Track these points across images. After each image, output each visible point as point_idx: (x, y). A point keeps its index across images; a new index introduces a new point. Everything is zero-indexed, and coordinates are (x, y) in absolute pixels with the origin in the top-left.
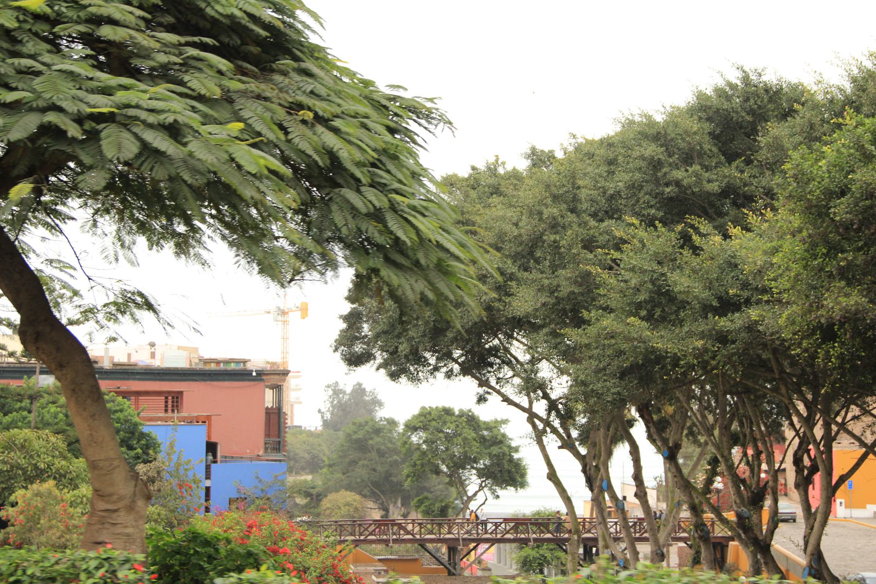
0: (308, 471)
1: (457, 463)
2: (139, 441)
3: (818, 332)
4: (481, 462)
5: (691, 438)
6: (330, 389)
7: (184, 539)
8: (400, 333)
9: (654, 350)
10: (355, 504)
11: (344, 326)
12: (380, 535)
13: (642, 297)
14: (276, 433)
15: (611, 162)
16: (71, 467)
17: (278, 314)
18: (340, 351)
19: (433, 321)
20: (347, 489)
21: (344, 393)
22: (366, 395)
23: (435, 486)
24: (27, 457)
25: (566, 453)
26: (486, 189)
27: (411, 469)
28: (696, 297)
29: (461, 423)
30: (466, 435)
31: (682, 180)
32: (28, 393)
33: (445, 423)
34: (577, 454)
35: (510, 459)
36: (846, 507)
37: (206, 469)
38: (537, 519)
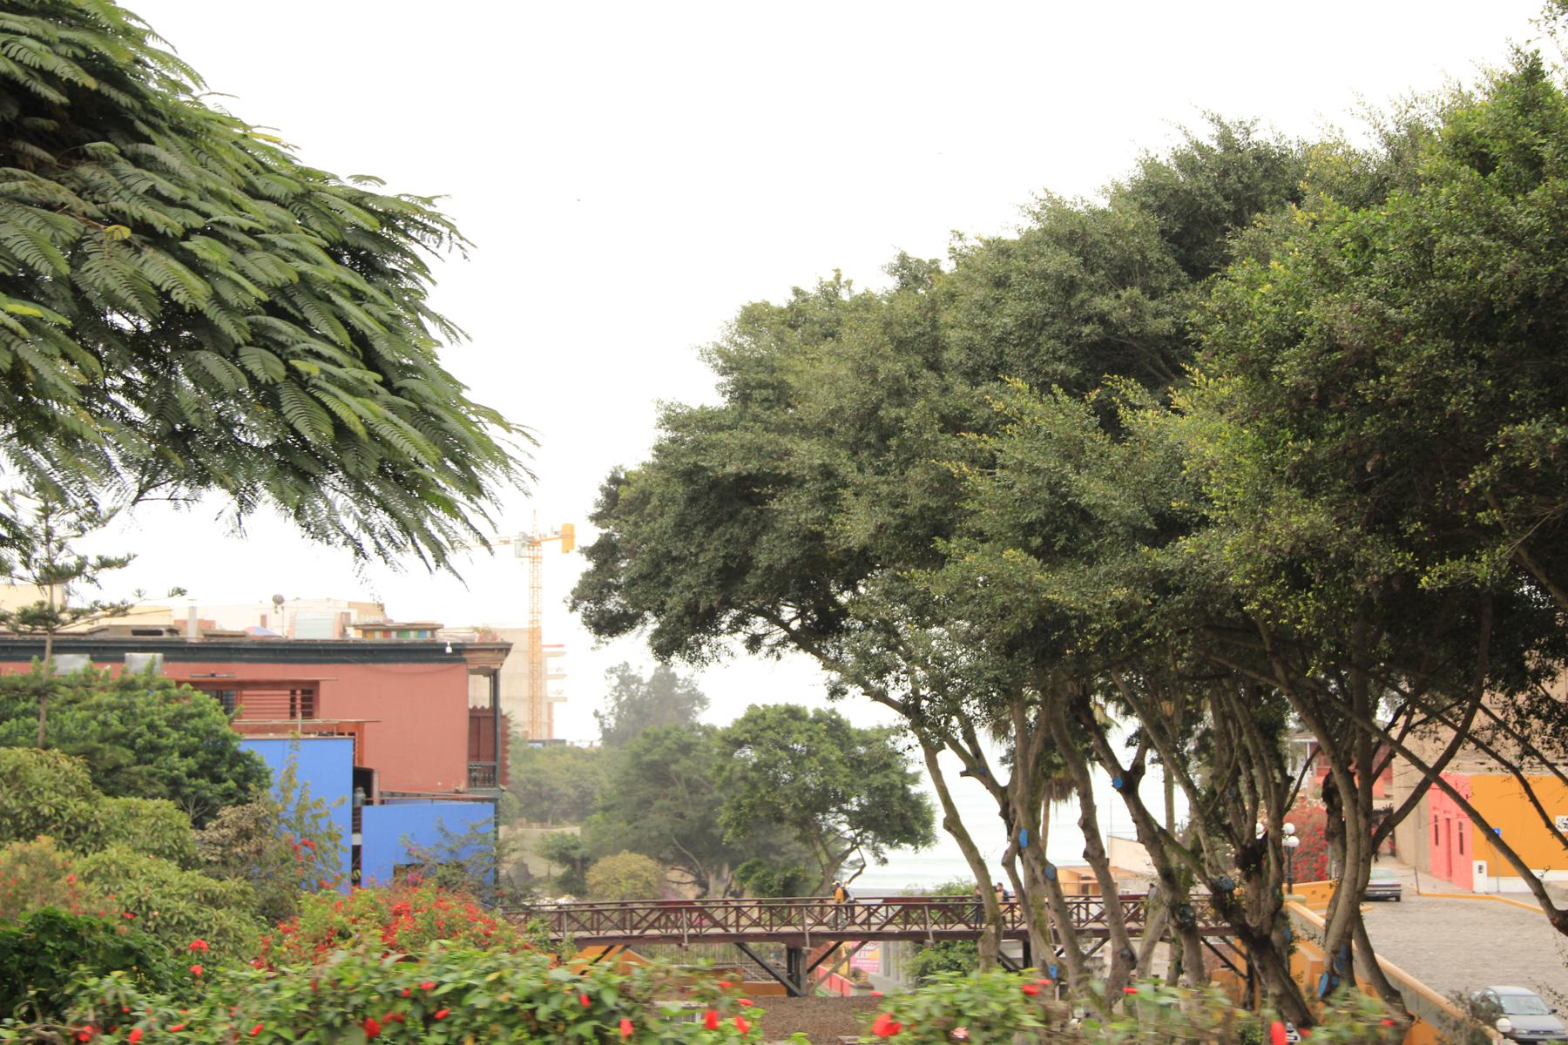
0: (574, 818)
1: (811, 802)
2: (232, 766)
3: (1283, 574)
4: (854, 799)
5: (1204, 756)
6: (614, 676)
7: (31, 927)
8: (669, 578)
9: (1052, 606)
10: (645, 874)
11: (590, 566)
12: (667, 928)
13: (1033, 515)
14: (491, 752)
15: (1001, 283)
16: (96, 812)
17: (523, 545)
18: (581, 610)
19: (724, 557)
20: (633, 850)
21: (639, 681)
22: (676, 685)
23: (789, 843)
24: (21, 796)
25: (973, 783)
26: (817, 328)
27: (732, 814)
28: (1117, 515)
29: (818, 734)
30: (825, 753)
31: (1109, 313)
32: (33, 685)
33: (789, 732)
34: (991, 784)
35: (903, 796)
36: (1489, 875)
37: (354, 815)
38: (946, 899)
